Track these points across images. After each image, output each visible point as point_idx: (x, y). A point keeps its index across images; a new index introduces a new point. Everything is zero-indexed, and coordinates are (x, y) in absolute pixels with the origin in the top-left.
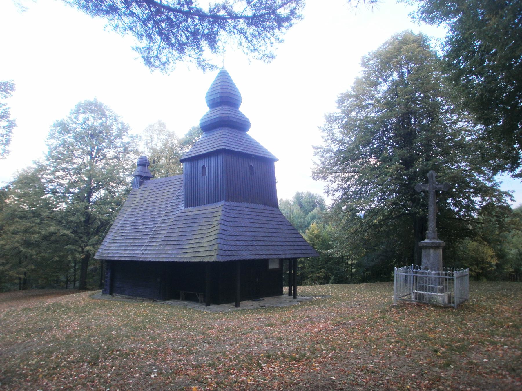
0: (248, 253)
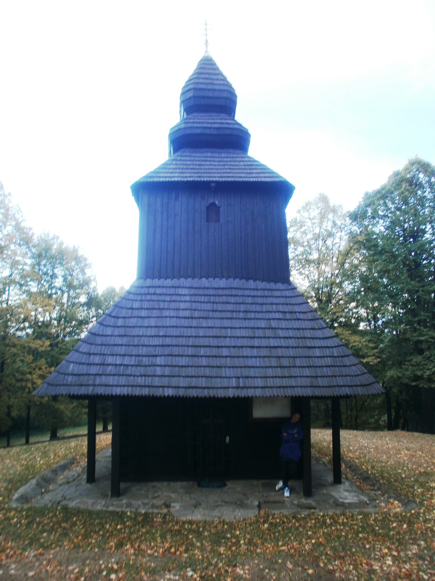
0: (123, 380)
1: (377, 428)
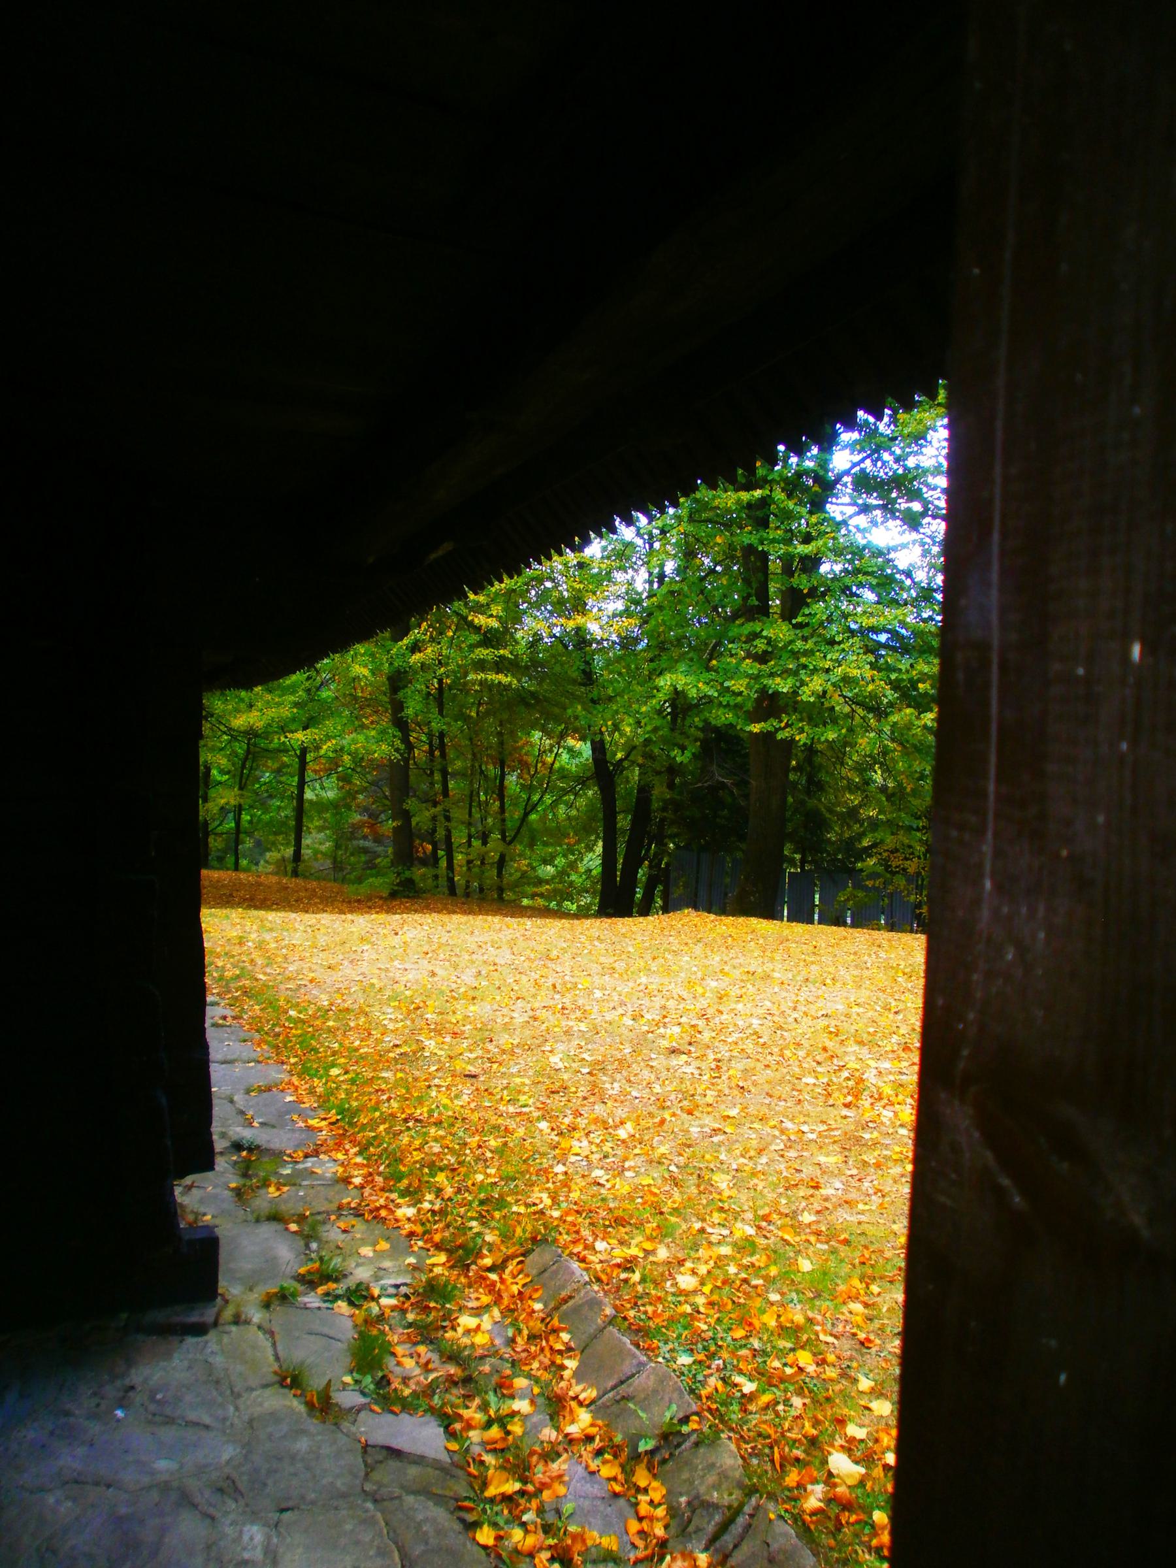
1: (553, 903)
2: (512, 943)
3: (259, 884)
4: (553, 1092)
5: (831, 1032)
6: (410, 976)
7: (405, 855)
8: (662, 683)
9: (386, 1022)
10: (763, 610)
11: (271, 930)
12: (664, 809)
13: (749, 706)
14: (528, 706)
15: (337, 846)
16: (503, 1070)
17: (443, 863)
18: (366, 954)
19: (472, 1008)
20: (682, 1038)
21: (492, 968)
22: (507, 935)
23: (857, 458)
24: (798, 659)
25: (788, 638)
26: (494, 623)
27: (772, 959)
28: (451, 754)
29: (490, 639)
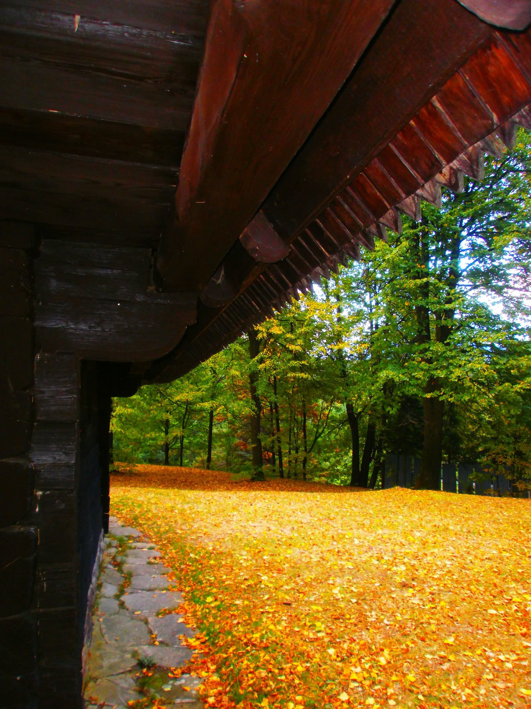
2: (310, 510)
3: (190, 473)
4: (336, 619)
5: (495, 572)
6: (257, 531)
7: (259, 460)
8: (382, 375)
9: (242, 561)
10: (427, 338)
11: (188, 503)
12: (381, 435)
13: (425, 384)
14: (316, 388)
15: (228, 454)
16: (306, 599)
17: (277, 462)
18: (235, 517)
19: (289, 551)
20: (407, 575)
21: (300, 525)
22: (308, 504)
23: (472, 261)
24: (448, 361)
25: (443, 350)
26: (298, 348)
27: (446, 517)
28: (281, 411)
29: (297, 356)
